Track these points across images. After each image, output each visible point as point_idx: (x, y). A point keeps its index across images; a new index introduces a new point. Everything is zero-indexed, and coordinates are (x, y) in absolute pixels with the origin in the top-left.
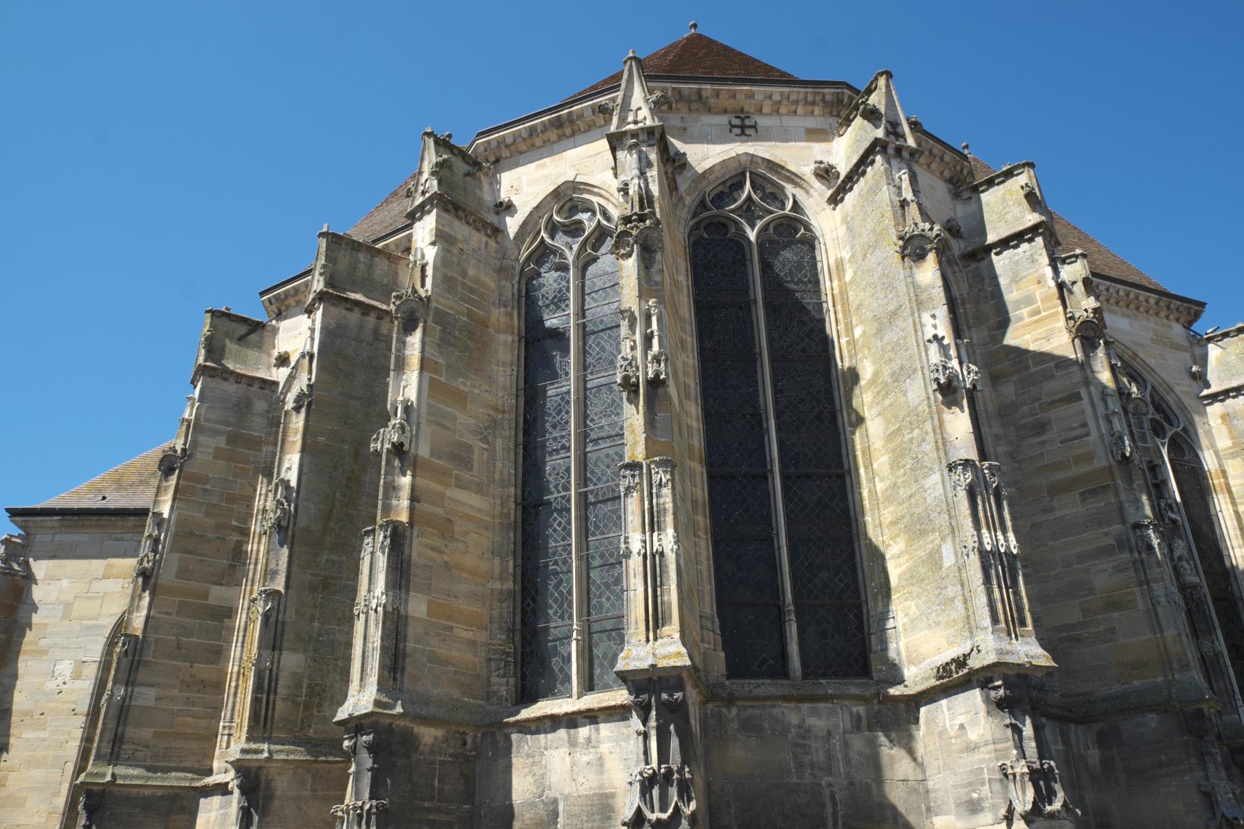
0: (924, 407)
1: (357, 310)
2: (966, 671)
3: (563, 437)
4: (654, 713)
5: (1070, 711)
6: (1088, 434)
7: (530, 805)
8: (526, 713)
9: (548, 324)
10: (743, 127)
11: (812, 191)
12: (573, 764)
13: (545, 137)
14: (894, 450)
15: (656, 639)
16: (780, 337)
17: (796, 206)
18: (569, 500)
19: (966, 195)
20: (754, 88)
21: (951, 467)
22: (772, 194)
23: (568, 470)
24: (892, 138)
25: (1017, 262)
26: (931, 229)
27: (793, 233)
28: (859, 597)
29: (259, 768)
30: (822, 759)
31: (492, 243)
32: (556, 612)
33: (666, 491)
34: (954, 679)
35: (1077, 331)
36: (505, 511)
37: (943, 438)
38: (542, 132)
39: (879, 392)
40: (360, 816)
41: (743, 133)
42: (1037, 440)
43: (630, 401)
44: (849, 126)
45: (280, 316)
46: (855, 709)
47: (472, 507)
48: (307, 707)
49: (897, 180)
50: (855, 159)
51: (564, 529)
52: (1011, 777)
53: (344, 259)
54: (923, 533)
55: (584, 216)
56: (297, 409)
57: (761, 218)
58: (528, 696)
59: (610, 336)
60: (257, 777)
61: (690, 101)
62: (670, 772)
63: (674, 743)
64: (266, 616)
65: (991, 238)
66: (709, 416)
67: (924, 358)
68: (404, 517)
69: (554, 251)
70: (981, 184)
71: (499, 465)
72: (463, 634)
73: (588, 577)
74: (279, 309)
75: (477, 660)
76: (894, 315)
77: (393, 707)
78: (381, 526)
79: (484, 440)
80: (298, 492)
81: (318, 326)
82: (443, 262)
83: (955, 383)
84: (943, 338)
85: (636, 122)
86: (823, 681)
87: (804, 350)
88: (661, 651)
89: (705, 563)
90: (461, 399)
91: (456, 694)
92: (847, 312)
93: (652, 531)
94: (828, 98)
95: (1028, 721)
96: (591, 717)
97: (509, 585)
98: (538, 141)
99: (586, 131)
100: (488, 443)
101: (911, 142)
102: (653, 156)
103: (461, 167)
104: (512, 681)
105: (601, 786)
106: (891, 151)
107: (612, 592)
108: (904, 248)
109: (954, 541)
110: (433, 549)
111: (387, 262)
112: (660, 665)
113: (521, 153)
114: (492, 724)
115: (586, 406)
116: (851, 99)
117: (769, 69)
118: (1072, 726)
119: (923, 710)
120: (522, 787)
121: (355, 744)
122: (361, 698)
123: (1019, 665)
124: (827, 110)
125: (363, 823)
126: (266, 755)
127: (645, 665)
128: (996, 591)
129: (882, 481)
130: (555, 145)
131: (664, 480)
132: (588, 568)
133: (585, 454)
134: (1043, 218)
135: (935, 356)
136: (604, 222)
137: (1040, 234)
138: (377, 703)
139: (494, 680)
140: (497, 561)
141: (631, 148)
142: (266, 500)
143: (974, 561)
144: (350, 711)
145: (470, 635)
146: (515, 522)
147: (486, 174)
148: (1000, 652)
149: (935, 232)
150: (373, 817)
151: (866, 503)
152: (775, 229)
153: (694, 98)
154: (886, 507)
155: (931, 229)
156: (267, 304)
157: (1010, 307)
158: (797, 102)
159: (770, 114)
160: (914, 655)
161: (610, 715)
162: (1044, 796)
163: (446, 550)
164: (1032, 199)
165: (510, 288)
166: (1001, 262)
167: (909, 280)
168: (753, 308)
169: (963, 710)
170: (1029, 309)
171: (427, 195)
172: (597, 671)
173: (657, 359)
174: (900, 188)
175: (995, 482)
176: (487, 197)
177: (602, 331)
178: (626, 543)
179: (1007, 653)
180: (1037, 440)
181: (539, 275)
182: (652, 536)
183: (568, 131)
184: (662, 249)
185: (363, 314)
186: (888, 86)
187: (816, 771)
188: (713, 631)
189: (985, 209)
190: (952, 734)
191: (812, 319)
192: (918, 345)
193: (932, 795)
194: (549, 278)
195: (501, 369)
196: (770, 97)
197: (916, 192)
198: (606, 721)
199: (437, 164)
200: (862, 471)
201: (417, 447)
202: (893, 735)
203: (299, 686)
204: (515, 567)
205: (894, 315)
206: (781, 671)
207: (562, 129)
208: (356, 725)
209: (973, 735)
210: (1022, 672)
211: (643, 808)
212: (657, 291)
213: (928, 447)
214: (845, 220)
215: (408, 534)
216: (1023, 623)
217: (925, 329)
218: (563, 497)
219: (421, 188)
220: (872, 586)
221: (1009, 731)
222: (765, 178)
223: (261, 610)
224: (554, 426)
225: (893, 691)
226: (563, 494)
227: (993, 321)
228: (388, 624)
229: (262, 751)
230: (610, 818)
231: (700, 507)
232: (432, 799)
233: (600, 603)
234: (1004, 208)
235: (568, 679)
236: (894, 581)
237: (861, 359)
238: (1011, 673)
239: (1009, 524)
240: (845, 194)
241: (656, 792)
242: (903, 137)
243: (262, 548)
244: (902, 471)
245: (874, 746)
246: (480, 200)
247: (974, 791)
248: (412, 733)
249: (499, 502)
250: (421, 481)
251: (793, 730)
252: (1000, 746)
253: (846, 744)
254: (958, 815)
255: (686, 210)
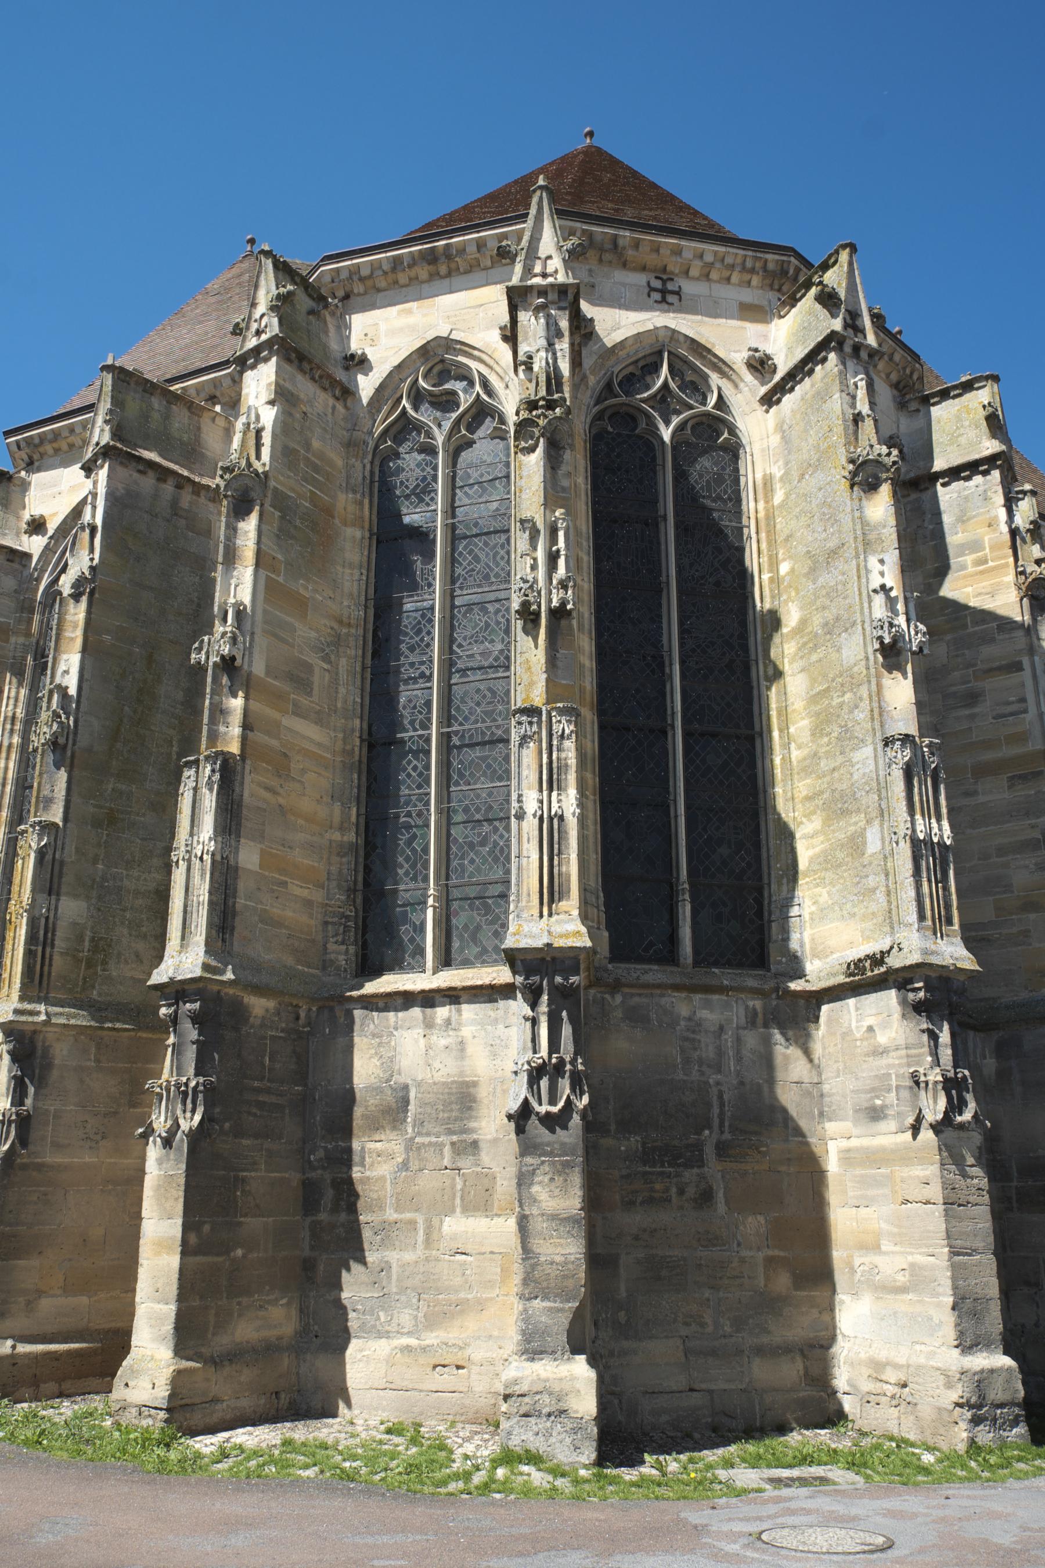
0: (861, 668)
1: (151, 473)
2: (883, 969)
3: (422, 663)
4: (545, 997)
5: (970, 1017)
6: (1026, 711)
7: (377, 1090)
8: (371, 988)
9: (407, 520)
10: (664, 292)
11: (741, 385)
12: (429, 1048)
13: (412, 273)
14: (817, 714)
15: (550, 915)
16: (691, 565)
17: (721, 400)
18: (428, 740)
19: (913, 406)
20: (683, 243)
21: (887, 742)
22: (693, 383)
23: (428, 704)
24: (850, 331)
25: (966, 498)
26: (889, 454)
27: (714, 438)
28: (760, 879)
29: (35, 1032)
30: (712, 1055)
31: (340, 407)
32: (407, 874)
33: (570, 745)
34: (866, 978)
35: (1028, 588)
36: (348, 747)
37: (880, 707)
38: (410, 266)
39: (805, 644)
40: (185, 1094)
41: (664, 300)
42: (967, 712)
43: (526, 631)
44: (793, 306)
45: (31, 466)
46: (751, 1003)
47: (312, 741)
48: (90, 964)
49: (852, 387)
50: (800, 353)
51: (420, 775)
52: (922, 1085)
53: (134, 404)
54: (845, 813)
55: (458, 386)
56: (76, 597)
57: (678, 413)
58: (371, 967)
59: (486, 544)
60: (32, 1041)
61: (602, 250)
62: (562, 1062)
63: (566, 1031)
64: (41, 853)
65: (939, 464)
66: (602, 654)
67: (866, 611)
68: (234, 748)
69: (418, 427)
70: (933, 395)
71: (342, 690)
72: (298, 891)
73: (449, 835)
74: (30, 457)
75: (313, 922)
76: (833, 554)
77: (223, 972)
78: (207, 758)
79: (326, 659)
80: (78, 702)
81: (102, 490)
82: (283, 427)
83: (901, 644)
84: (891, 589)
85: (544, 275)
86: (716, 971)
87: (717, 584)
88: (557, 929)
89: (592, 827)
90: (301, 606)
91: (290, 961)
92: (772, 542)
93: (551, 789)
94: (771, 266)
95: (946, 1027)
96: (453, 996)
97: (351, 837)
98: (403, 278)
99: (465, 273)
100: (330, 662)
101: (871, 340)
102: (564, 324)
103: (304, 302)
104: (352, 949)
105: (462, 1073)
106: (848, 349)
107: (477, 853)
108: (854, 474)
109: (881, 826)
110: (268, 789)
111: (187, 414)
112: (556, 945)
113: (379, 290)
114: (332, 998)
115: (452, 627)
116: (798, 270)
117: (666, 199)
118: (971, 1033)
119: (825, 1008)
120: (365, 1069)
121: (176, 1012)
122: (184, 959)
123: (943, 967)
124: (768, 281)
125: (189, 1101)
126: (43, 1017)
127: (539, 943)
128: (925, 885)
129: (799, 747)
130: (425, 286)
131: (567, 731)
132: (449, 824)
133: (450, 686)
134: (1004, 447)
135: (879, 609)
136: (485, 397)
137: (998, 467)
138: (206, 967)
139: (331, 947)
140: (337, 807)
141: (538, 309)
142: (15, 706)
143: (905, 850)
144: (170, 974)
145: (305, 893)
146: (360, 761)
147: (333, 314)
148: (925, 952)
149: (893, 458)
150: (201, 1096)
151: (778, 772)
152: (693, 427)
153: (608, 246)
154: (800, 780)
155: (889, 454)
156: (15, 448)
157: (951, 552)
158: (732, 267)
159: (698, 279)
160: (820, 948)
161: (475, 995)
162: (955, 1106)
163: (281, 791)
164: (995, 424)
165: (361, 468)
166: (947, 495)
167: (857, 514)
168: (662, 526)
169: (874, 1011)
170: (974, 556)
171: (264, 337)
172: (456, 944)
173: (563, 585)
174: (854, 397)
175: (934, 762)
176: (334, 345)
177: (476, 536)
178: (519, 801)
179: (933, 953)
180: (967, 712)
181: (397, 455)
182: (550, 796)
183: (443, 269)
184: (572, 447)
185: (159, 480)
186: (851, 264)
187: (704, 1068)
188: (597, 907)
189: (935, 427)
190: (858, 1036)
191: (730, 546)
192: (860, 594)
193: (826, 1099)
194: (410, 461)
195: (348, 571)
196: (701, 256)
197: (872, 404)
198: (470, 1002)
199: (279, 297)
200: (776, 734)
201: (251, 662)
202: (790, 1033)
203: (80, 938)
204: (358, 815)
205: (833, 554)
206: (669, 956)
207: (431, 260)
208: (178, 991)
209: (882, 1038)
210: (945, 974)
211: (531, 1099)
212: (564, 498)
213: (862, 716)
214: (780, 427)
215: (239, 768)
216: (949, 922)
217: (872, 576)
218: (420, 736)
219: (254, 326)
220: (778, 867)
221: (925, 1037)
222: (685, 361)
223: (34, 845)
224: (412, 649)
225: (794, 986)
226: (420, 732)
227: (930, 567)
228: (217, 874)
229: (38, 1013)
230: (470, 1108)
231: (589, 762)
232: (262, 1079)
233: (462, 865)
234: (958, 429)
235: (421, 951)
236: (803, 864)
237: (786, 602)
238: (933, 975)
239: (944, 811)
240: (783, 394)
241: (544, 1083)
242: (863, 331)
243: (11, 765)
244: (826, 739)
245: (767, 1043)
246: (325, 347)
247: (878, 1097)
248: (241, 1003)
249: (341, 735)
250: (254, 705)
251: (683, 1023)
252: (913, 1052)
253: (738, 1040)
254: (856, 1122)
255: (589, 393)
